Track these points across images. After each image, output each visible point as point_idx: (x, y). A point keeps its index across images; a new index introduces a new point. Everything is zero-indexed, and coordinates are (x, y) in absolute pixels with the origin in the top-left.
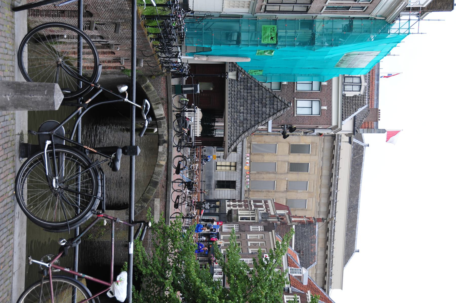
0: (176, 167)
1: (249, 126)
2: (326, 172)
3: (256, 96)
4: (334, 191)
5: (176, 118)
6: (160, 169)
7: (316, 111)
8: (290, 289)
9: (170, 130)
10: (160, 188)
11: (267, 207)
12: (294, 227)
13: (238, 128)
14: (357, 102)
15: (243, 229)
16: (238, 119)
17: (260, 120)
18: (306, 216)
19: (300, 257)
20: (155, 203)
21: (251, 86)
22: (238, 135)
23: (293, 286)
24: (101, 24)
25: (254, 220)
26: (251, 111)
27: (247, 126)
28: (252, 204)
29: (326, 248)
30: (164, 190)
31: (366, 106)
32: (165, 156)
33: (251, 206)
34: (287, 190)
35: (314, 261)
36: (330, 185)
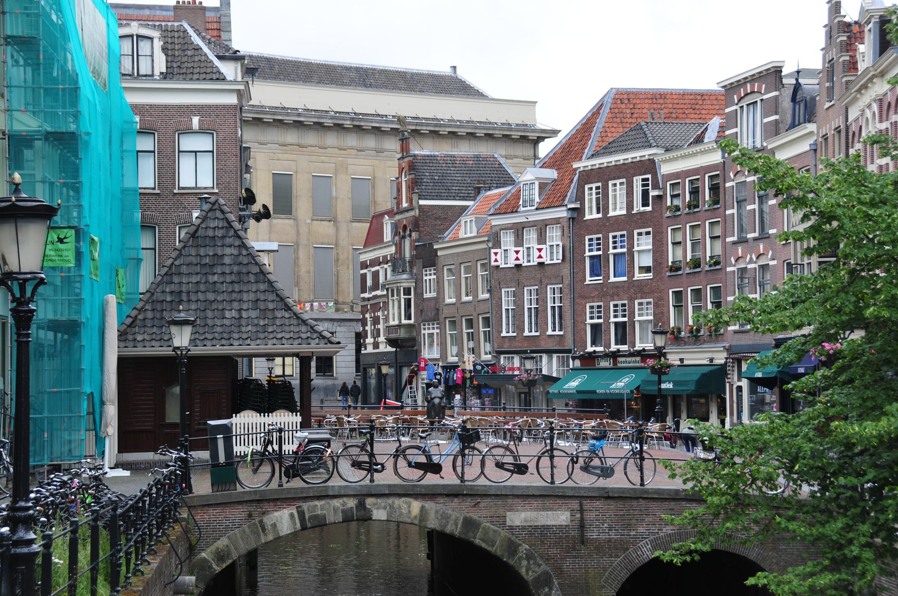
0: (422, 472)
1: (272, 297)
2: (291, 137)
3: (194, 279)
4: (332, 118)
5: (298, 478)
6: (432, 515)
7: (204, 143)
8: (570, 206)
9: (331, 493)
10: (481, 513)
11: (375, 262)
12: (422, 202)
13: (278, 322)
14: (177, 47)
15: (431, 314)
16: (256, 321)
17: (256, 270)
18: (397, 176)
19: (490, 187)
20: (518, 523)
21: (172, 292)
22: (295, 322)
23: (563, 200)
25: (409, 289)
26: (233, 291)
27: (273, 301)
28: (371, 296)
29: (453, 134)
30: (484, 502)
31: (186, 26)
32: (399, 502)
33: (376, 297)
34: (334, 220)
35: (492, 159)
36: (319, 126)
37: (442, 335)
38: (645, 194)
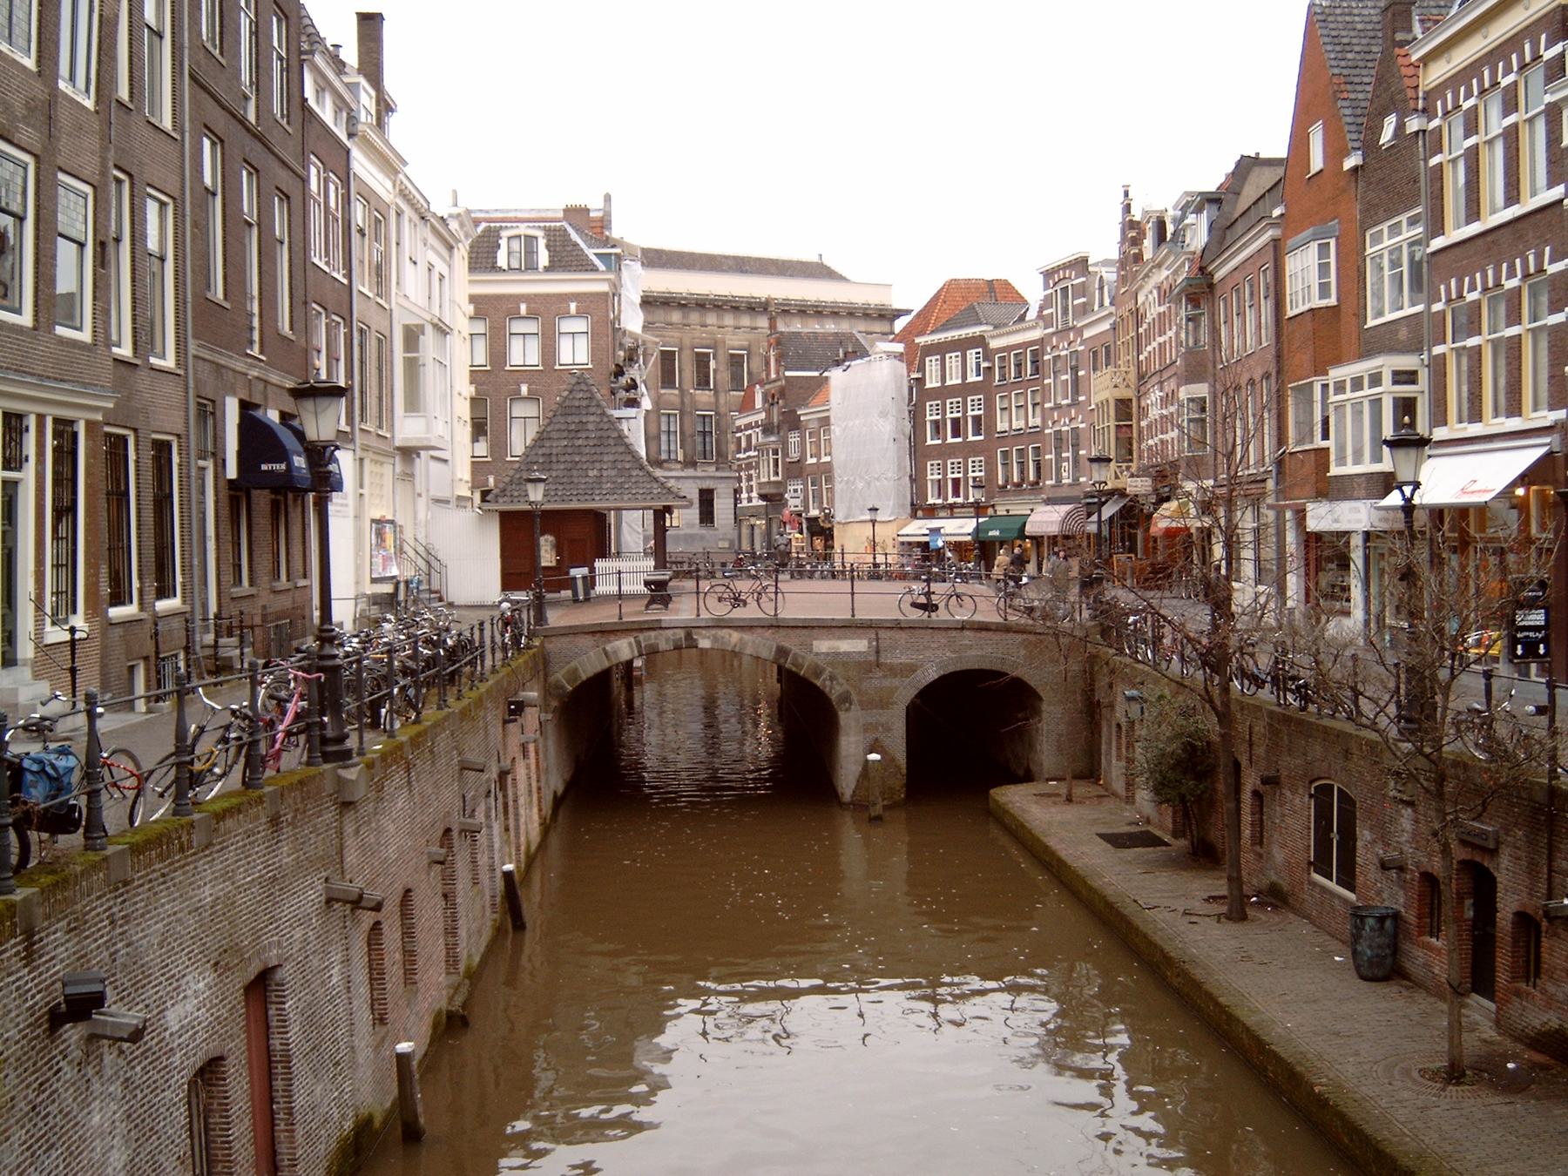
1: (629, 458)
7: (580, 325)
10: (791, 642)
11: (749, 426)
12: (788, 374)
17: (615, 435)
24: (464, 802)
33: (749, 457)
37: (805, 490)
38: (978, 365)
